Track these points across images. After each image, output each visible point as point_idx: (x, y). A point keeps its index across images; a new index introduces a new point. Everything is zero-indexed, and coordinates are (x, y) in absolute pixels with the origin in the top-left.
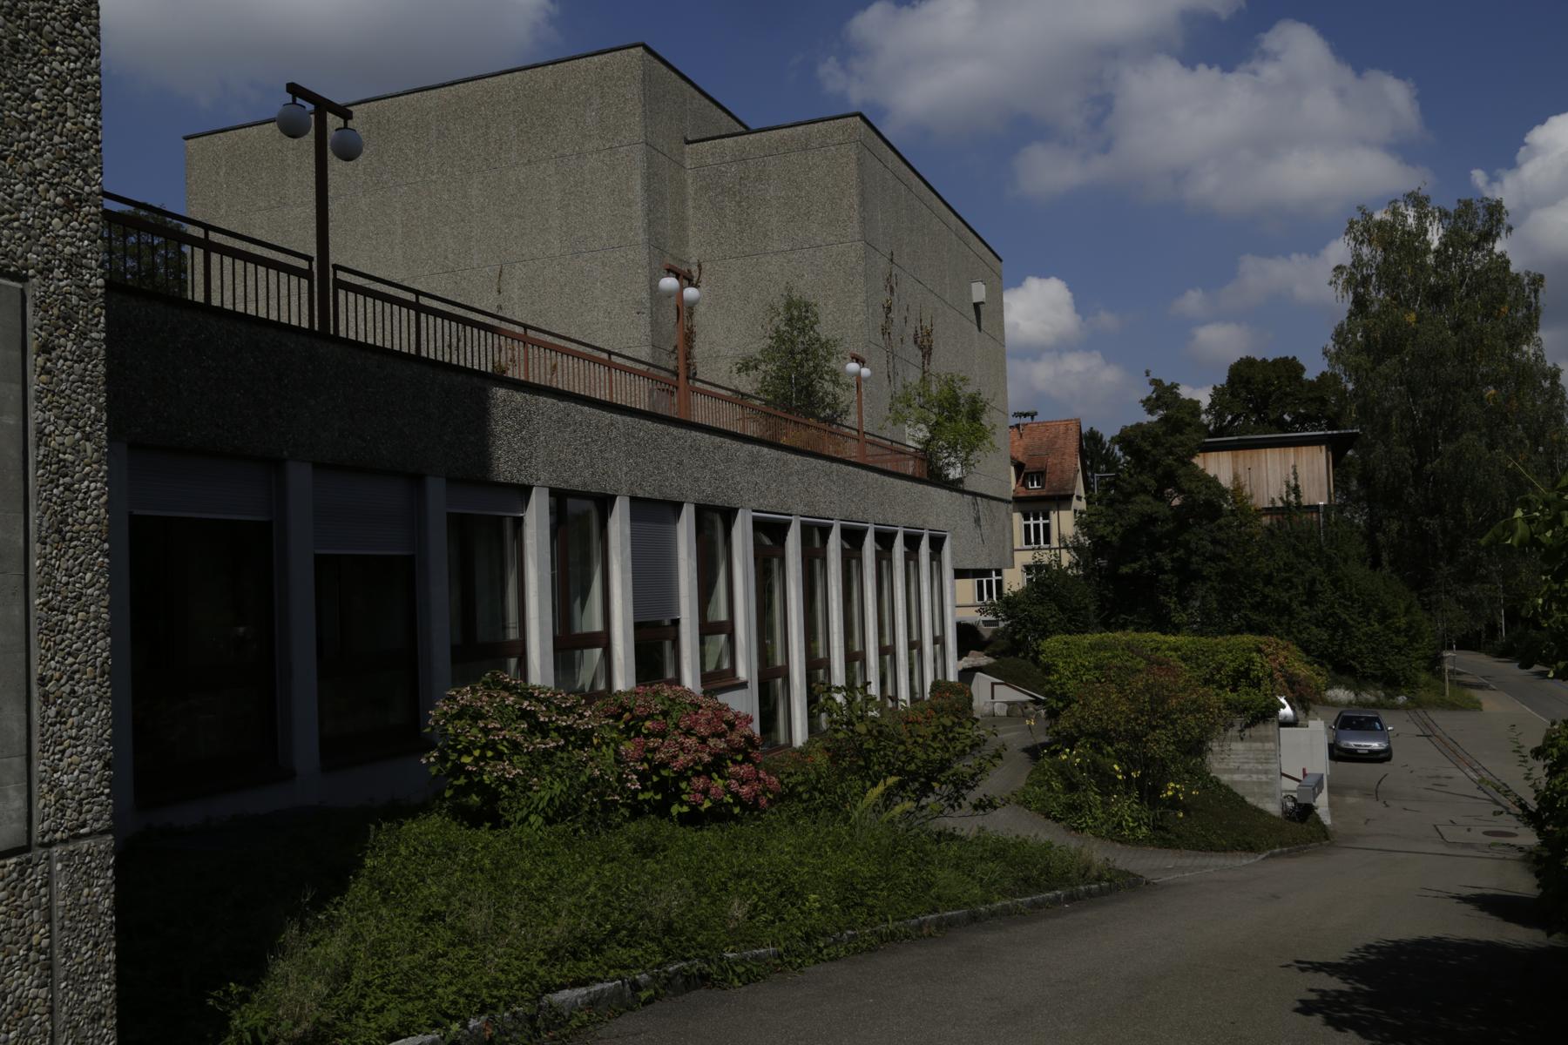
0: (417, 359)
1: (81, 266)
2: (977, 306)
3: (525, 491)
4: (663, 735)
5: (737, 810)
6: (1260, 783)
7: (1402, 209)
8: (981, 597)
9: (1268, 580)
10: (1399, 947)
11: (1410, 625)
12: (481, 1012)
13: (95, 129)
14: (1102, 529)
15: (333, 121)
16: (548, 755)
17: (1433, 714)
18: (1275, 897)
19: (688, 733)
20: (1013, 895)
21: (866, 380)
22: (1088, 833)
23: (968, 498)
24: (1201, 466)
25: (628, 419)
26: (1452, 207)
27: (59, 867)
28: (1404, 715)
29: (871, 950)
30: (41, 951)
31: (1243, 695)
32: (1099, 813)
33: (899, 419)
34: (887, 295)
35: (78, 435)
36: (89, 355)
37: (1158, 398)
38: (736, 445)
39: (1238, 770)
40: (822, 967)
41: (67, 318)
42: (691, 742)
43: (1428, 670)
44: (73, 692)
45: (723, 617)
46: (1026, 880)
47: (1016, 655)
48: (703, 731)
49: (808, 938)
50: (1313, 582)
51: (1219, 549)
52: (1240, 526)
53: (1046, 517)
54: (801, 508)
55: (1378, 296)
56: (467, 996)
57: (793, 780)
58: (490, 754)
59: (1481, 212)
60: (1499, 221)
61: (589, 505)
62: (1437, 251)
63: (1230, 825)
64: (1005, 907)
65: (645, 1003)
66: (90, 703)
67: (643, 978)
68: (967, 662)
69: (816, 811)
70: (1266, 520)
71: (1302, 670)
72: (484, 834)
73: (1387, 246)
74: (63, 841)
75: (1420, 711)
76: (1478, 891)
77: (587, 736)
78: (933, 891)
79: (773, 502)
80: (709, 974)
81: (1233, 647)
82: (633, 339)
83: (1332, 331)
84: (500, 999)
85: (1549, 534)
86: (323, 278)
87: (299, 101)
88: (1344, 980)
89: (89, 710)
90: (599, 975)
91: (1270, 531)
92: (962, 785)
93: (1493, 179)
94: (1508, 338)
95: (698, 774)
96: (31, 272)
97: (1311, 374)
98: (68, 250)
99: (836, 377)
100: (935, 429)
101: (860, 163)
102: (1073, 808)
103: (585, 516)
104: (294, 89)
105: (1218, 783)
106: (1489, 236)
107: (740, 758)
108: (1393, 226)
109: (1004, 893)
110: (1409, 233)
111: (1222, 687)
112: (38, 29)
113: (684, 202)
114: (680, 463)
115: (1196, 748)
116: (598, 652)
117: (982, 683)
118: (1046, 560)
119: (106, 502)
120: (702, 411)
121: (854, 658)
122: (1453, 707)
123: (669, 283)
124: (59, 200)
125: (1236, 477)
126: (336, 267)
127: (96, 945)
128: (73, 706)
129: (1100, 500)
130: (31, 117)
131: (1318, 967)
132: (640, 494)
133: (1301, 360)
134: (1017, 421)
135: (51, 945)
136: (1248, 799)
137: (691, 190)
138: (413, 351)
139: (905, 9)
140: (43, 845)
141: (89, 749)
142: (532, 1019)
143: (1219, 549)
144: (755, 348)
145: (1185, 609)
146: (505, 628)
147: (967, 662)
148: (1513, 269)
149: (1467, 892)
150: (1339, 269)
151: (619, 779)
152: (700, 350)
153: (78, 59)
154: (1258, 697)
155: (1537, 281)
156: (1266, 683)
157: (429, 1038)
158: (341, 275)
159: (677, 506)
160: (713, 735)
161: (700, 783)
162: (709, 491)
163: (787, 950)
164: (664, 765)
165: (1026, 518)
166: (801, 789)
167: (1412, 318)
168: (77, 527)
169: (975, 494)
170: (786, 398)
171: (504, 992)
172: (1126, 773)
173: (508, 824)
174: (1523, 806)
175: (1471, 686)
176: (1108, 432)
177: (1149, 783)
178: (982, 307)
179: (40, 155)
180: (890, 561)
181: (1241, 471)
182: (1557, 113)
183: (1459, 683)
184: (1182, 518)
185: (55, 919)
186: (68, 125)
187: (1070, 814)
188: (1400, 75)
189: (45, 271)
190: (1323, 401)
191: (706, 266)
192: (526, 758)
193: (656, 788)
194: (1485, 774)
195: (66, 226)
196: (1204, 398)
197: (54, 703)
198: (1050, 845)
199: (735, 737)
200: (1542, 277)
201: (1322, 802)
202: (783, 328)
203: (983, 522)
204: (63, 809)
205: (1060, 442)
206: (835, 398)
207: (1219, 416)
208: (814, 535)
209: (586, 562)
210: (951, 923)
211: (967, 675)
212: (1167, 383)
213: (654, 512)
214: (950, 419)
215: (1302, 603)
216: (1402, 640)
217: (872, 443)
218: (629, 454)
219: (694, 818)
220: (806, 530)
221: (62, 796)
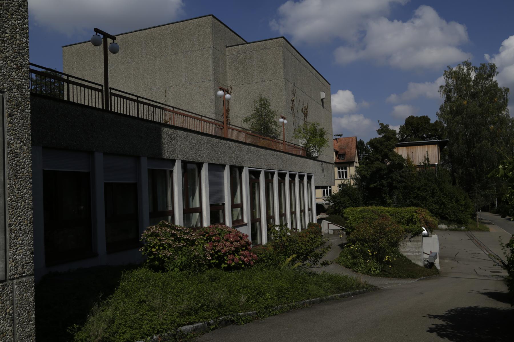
0: (138, 118)
1: (22, 88)
2: (322, 100)
3: (173, 161)
4: (218, 241)
5: (243, 266)
6: (416, 256)
7: (462, 67)
8: (324, 195)
9: (419, 189)
10: (462, 310)
11: (466, 204)
12: (158, 333)
13: (27, 43)
14: (364, 173)
15: (109, 41)
16: (180, 248)
17: (473, 233)
18: (421, 293)
19: (227, 240)
20: (335, 293)
21: (286, 124)
25: (207, 138)
26: (478, 66)
27: (16, 287)
28: (464, 233)
30: (10, 315)
31: (411, 227)
32: (363, 266)
33: (297, 137)
35: (22, 144)
37: (382, 130)
38: (243, 146)
39: (409, 251)
40: (271, 318)
41: (18, 105)
42: (228, 243)
44: (20, 229)
45: (239, 202)
46: (339, 288)
48: (232, 240)
49: (266, 308)
50: (433, 189)
51: (403, 179)
52: (409, 171)
53: (346, 169)
54: (264, 167)
55: (454, 95)
56: (153, 328)
57: (262, 256)
58: (161, 248)
59: (488, 68)
60: (494, 70)
61: (195, 166)
62: (473, 81)
63: (407, 270)
65: (212, 330)
66: (26, 232)
67: (211, 321)
68: (320, 217)
69: (269, 266)
70: (418, 169)
71: (430, 218)
72: (159, 274)
73: (457, 79)
74: (17, 278)
75: (469, 232)
76: (489, 291)
77: (194, 241)
78: (308, 292)
79: (255, 164)
80: (233, 320)
81: (407, 211)
83: (439, 107)
84: (164, 329)
86: (107, 92)
87: (98, 34)
88: (444, 321)
89: (26, 234)
90: (197, 321)
91: (419, 173)
92: (317, 257)
93: (492, 57)
94: (497, 109)
95: (230, 254)
96: (5, 90)
97: (432, 121)
98: (18, 83)
99: (276, 123)
100: (309, 140)
102: (355, 264)
103: (193, 170)
104: (97, 30)
105: (402, 256)
106: (491, 75)
107: (244, 249)
108: (459, 72)
109: (332, 293)
110: (464, 75)
111: (404, 224)
112: (7, 10)
114: (225, 152)
115: (395, 244)
116: (198, 214)
117: (325, 223)
118: (345, 183)
119: (31, 166)
120: (232, 135)
121: (282, 215)
122: (480, 230)
123: (221, 93)
125: (408, 155)
126: (111, 88)
127: (28, 312)
128: (20, 233)
129: (363, 163)
130: (5, 39)
133: (429, 117)
134: (336, 137)
135: (13, 313)
136: (413, 261)
137: (228, 63)
138: (136, 116)
139: (297, 3)
140: (10, 279)
141: (26, 248)
142: (174, 335)
143: (403, 179)
144: (249, 114)
145: (391, 199)
146: (167, 206)
147: (320, 217)
148: (499, 86)
149: (484, 291)
150: (441, 87)
151: (204, 256)
152: (231, 115)
154: (415, 227)
155: (507, 90)
156: (418, 223)
158: (112, 91)
159: (224, 166)
161: (231, 257)
162: (234, 161)
163: (259, 312)
164: (219, 251)
165: (339, 169)
166: (264, 259)
168: (21, 174)
171: (165, 327)
172: (372, 253)
173: (167, 271)
174: (503, 263)
175: (486, 223)
176: (366, 141)
179: (8, 51)
180: (294, 184)
181: (409, 153)
183: (482, 222)
184: (390, 169)
185: (15, 304)
186: (18, 41)
187: (354, 266)
188: (461, 23)
189: (10, 90)
190: (436, 130)
191: (233, 87)
193: (217, 259)
196: (397, 129)
197: (14, 233)
198: (347, 277)
199: (242, 242)
200: (508, 89)
201: (437, 262)
202: (259, 107)
203: (325, 171)
204: (17, 268)
205: (350, 144)
206: (276, 130)
207: (402, 135)
208: (269, 175)
210: (314, 303)
211: (320, 221)
212: (385, 124)
213: (216, 168)
215: (430, 197)
216: (463, 208)
218: (208, 149)
219: (229, 269)
220: (266, 174)
221: (17, 263)
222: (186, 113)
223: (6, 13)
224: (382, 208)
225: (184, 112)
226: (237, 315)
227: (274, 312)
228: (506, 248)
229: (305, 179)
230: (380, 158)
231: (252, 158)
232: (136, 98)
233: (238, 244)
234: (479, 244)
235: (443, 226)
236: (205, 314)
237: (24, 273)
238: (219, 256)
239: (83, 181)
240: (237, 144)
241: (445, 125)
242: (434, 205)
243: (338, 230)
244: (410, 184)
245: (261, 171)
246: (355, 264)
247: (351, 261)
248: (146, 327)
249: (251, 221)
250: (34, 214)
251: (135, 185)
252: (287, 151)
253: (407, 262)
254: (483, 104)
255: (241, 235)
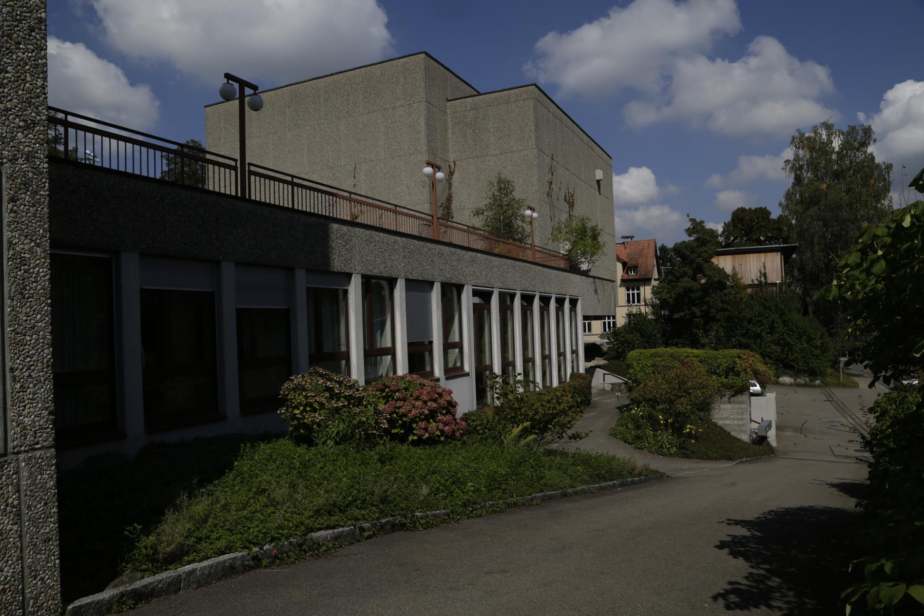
0: (293, 210)
1: (35, 157)
2: (598, 182)
3: (349, 276)
4: (404, 400)
5: (442, 439)
6: (739, 425)
7: (820, 131)
8: (605, 330)
9: (750, 321)
10: (788, 512)
11: (822, 344)
12: (271, 541)
13: (44, 87)
14: (665, 296)
15: (248, 91)
16: (337, 410)
17: (833, 390)
18: (733, 484)
19: (417, 399)
21: (536, 219)
22: (646, 451)
23: (591, 279)
24: (716, 263)
26: (845, 129)
27: (23, 464)
28: (818, 390)
29: (501, 511)
30: (13, 507)
31: (731, 380)
32: (651, 440)
33: (555, 239)
34: (550, 176)
35: (32, 244)
36: (39, 203)
37: (694, 228)
38: (463, 252)
39: (727, 418)
40: (470, 521)
41: (26, 184)
42: (419, 403)
43: (831, 367)
44: (30, 376)
47: (619, 359)
48: (425, 398)
49: (465, 505)
50: (773, 322)
51: (725, 306)
52: (736, 293)
53: (638, 289)
54: (499, 285)
55: (807, 175)
58: (308, 409)
59: (860, 132)
60: (870, 137)
62: (838, 152)
64: (583, 490)
65: (367, 538)
66: (40, 382)
67: (366, 525)
69: (486, 439)
70: (749, 291)
71: (762, 368)
72: (302, 450)
74: (25, 451)
75: (827, 389)
76: (842, 481)
77: (360, 400)
79: (484, 281)
81: (727, 355)
82: (421, 202)
83: (784, 193)
84: (282, 535)
85: (849, 293)
86: (243, 170)
87: (230, 82)
88: (749, 530)
90: (342, 523)
91: (751, 296)
92: (564, 427)
93: (869, 117)
94: (874, 197)
95: (422, 420)
96: (5, 161)
97: (774, 215)
98: (26, 149)
99: (523, 217)
100: (574, 244)
101: (535, 109)
102: (638, 437)
103: (381, 288)
104: (228, 76)
105: (716, 425)
106: (864, 144)
107: (444, 412)
109: (584, 482)
111: (720, 376)
112: (10, 36)
113: (446, 130)
114: (433, 261)
115: (705, 407)
116: (389, 357)
117: (599, 373)
118: (634, 312)
119: (50, 279)
120: (457, 238)
121: (528, 360)
122: (844, 386)
123: (428, 170)
124: (21, 124)
125: (734, 269)
126: (250, 164)
127: (46, 504)
128: (30, 383)
129: (664, 280)
130: (5, 81)
131: (737, 523)
132: (411, 277)
133: (769, 209)
134: (623, 240)
135: (19, 504)
136: (732, 433)
137: (450, 125)
138: (290, 206)
140: (14, 453)
141: (40, 405)
142: (301, 545)
143: (725, 306)
144: (482, 204)
145: (707, 336)
146: (339, 345)
148: (877, 161)
149: (835, 482)
150: (787, 161)
151: (376, 422)
152: (455, 205)
153: (33, 51)
154: (738, 382)
155: (889, 167)
156: (743, 374)
157: (240, 554)
158: (252, 168)
159: (431, 284)
160: (430, 400)
161: (423, 424)
162: (448, 275)
163: (452, 512)
164: (405, 415)
165: (628, 290)
167: (824, 186)
168: (32, 291)
169: (594, 277)
170: (498, 229)
171: (286, 532)
172: (666, 420)
173: (317, 444)
174: (863, 437)
177: (680, 425)
178: (601, 183)
179: (11, 100)
181: (737, 265)
182: (900, 82)
183: (848, 374)
185: (22, 491)
186: (27, 85)
187: (636, 441)
188: (821, 63)
189: (13, 160)
190: (780, 230)
191: (458, 163)
192: (327, 411)
193: (401, 427)
194: (857, 420)
195: (25, 137)
197: (19, 381)
199: (442, 401)
200: (891, 165)
201: (772, 435)
202: (496, 193)
203: (599, 292)
204: (25, 435)
205: (646, 251)
206: (523, 229)
207: (727, 238)
208: (506, 300)
209: (383, 314)
210: (551, 498)
211: (590, 371)
212: (698, 220)
213: (418, 287)
214: (581, 239)
215: (767, 333)
216: (818, 352)
217: (539, 251)
218: (405, 257)
220: (502, 296)
221: (25, 428)
222: (385, 205)
223: (7, 41)
224: (689, 350)
225: (381, 204)
226: (413, 516)
227: (479, 512)
228: (869, 415)
229: (567, 305)
230: (690, 272)
231: (476, 272)
232: (289, 179)
233: (435, 405)
234: (841, 408)
235: (786, 379)
236: (357, 513)
237: (37, 443)
238: (404, 422)
239: (205, 305)
240: (453, 249)
241: (794, 222)
242: (774, 347)
243: (620, 384)
244: (736, 313)
245: (492, 292)
246: (638, 437)
247: (633, 433)
248: (254, 531)
249: (476, 369)
250: (54, 354)
251: (288, 310)
252: (537, 260)
253: (723, 434)
254: (852, 189)
255: (440, 390)
